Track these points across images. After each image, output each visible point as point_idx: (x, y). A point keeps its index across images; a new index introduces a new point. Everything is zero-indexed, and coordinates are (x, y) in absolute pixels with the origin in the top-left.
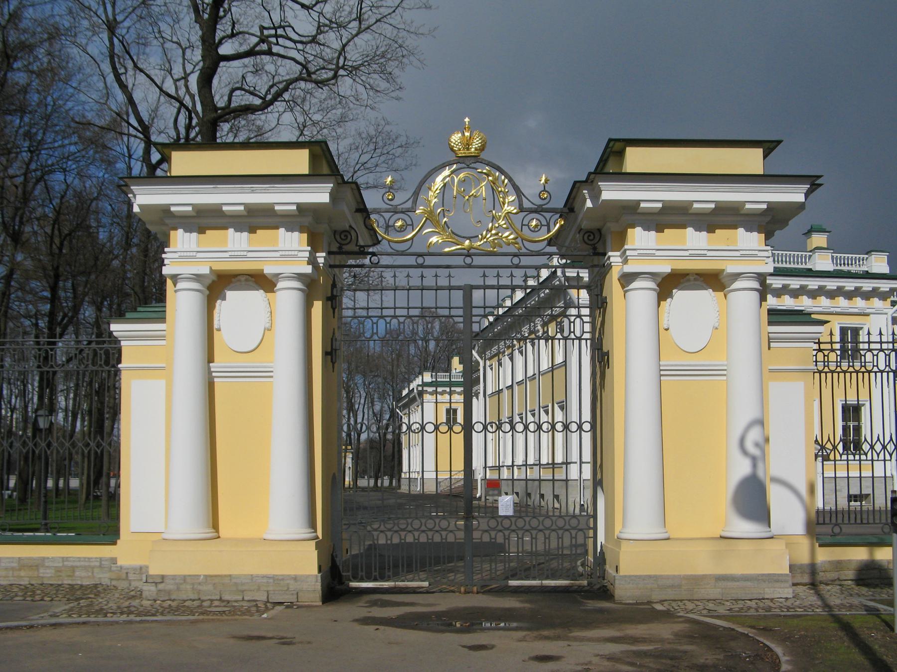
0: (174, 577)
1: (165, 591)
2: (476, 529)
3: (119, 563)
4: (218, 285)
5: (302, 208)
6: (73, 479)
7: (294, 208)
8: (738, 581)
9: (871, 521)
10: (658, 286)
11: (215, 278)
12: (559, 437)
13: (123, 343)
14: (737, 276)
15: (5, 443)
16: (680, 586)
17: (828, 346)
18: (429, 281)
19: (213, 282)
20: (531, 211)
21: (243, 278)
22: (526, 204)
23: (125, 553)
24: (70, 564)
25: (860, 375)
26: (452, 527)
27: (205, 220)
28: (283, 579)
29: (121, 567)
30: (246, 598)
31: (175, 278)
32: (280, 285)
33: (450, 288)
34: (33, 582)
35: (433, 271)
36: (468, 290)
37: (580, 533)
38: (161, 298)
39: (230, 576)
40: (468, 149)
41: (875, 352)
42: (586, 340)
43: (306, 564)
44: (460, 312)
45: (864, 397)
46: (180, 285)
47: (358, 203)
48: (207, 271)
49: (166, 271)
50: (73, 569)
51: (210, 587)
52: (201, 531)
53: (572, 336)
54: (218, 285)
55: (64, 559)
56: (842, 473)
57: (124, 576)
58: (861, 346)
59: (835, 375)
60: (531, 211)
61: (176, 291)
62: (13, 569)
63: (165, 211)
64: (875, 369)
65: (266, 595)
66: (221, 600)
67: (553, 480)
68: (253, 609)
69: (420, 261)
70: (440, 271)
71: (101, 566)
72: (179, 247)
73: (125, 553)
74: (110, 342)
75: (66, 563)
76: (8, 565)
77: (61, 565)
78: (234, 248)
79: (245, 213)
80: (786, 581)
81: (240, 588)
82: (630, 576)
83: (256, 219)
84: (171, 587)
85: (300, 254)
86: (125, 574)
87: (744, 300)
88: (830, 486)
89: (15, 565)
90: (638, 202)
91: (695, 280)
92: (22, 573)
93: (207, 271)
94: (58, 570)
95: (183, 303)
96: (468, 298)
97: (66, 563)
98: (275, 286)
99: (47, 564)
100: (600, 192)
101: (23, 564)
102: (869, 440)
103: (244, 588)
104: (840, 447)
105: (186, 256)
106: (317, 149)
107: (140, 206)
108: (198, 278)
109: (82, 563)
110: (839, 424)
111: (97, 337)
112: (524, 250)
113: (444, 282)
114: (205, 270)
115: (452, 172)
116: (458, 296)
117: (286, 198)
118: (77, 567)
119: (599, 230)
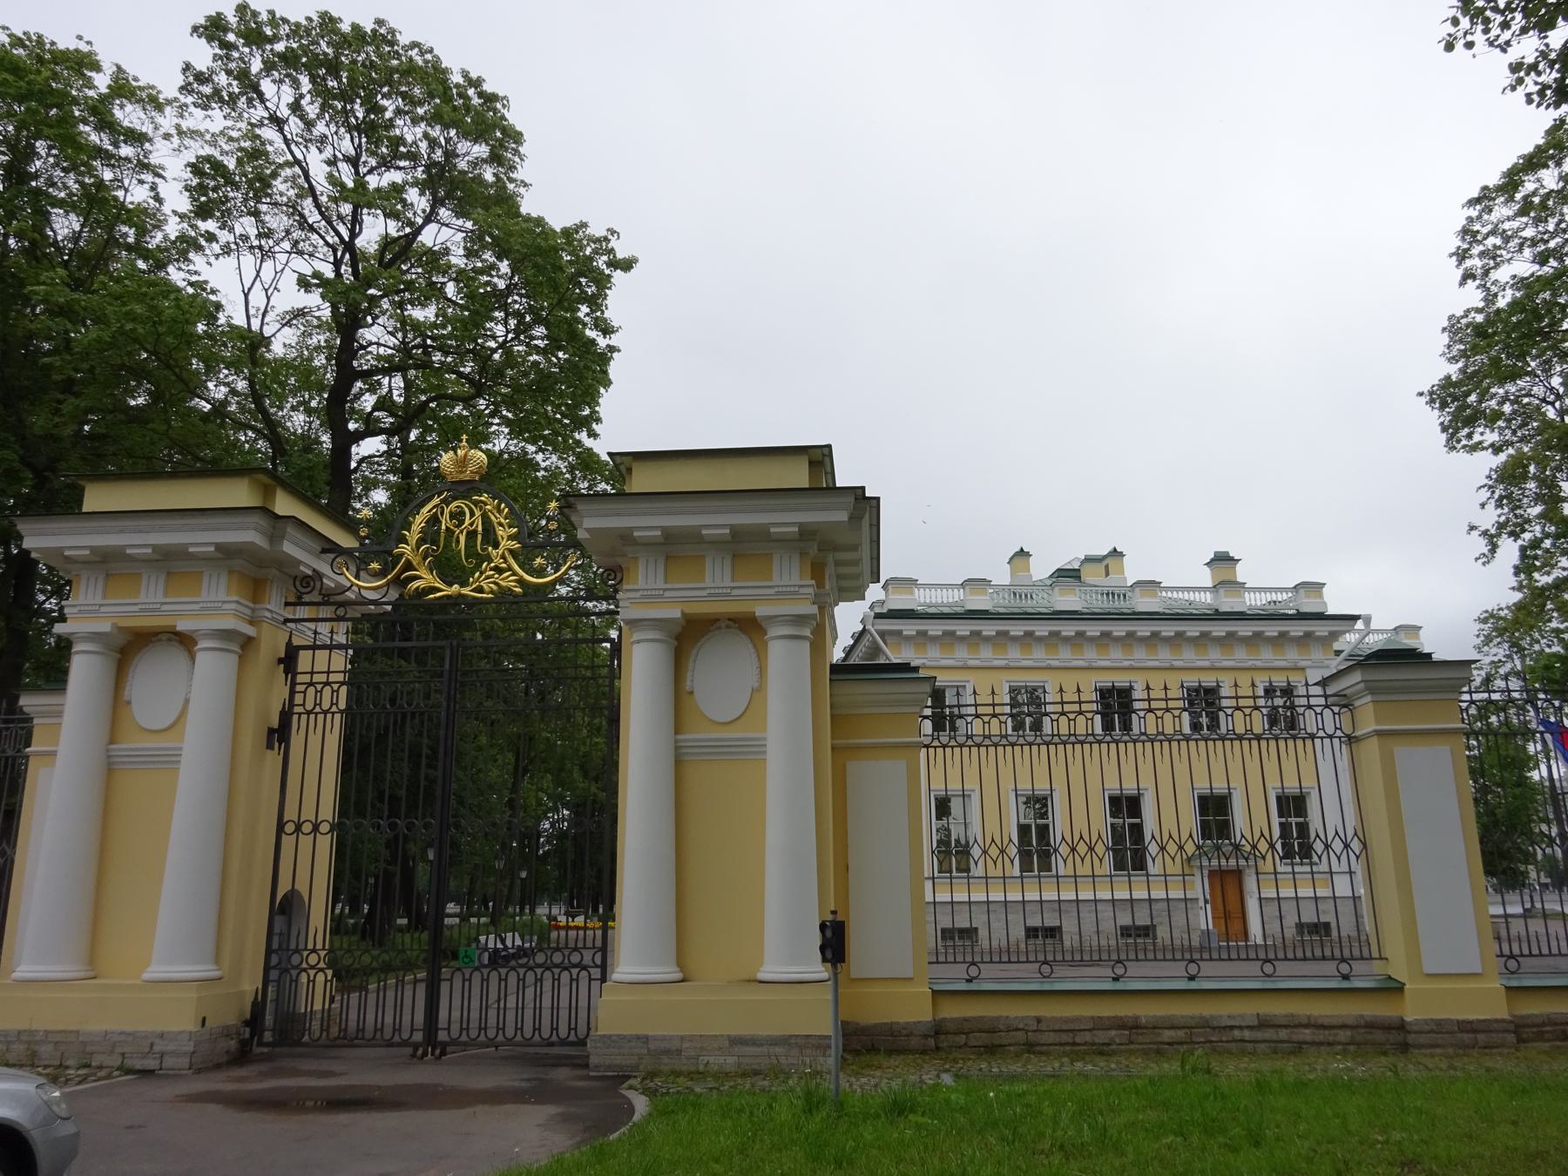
4: (129, 648)
14: (771, 618)
16: (679, 1052)
17: (1250, 702)
21: (164, 637)
37: (584, 973)
41: (1089, 715)
45: (1147, 783)
51: (50, 1048)
52: (670, 972)
53: (318, 709)
56: (1288, 892)
58: (1298, 701)
63: (626, 537)
64: (1321, 733)
67: (1041, 901)
72: (641, 584)
78: (148, 603)
81: (89, 1049)
83: (172, 565)
85: (803, 590)
87: (211, 669)
88: (1271, 910)
90: (631, 529)
91: (728, 627)
95: (84, 670)
100: (283, 537)
102: (1176, 837)
104: (976, 852)
105: (87, 615)
107: (587, 530)
110: (1276, 820)
115: (442, 501)
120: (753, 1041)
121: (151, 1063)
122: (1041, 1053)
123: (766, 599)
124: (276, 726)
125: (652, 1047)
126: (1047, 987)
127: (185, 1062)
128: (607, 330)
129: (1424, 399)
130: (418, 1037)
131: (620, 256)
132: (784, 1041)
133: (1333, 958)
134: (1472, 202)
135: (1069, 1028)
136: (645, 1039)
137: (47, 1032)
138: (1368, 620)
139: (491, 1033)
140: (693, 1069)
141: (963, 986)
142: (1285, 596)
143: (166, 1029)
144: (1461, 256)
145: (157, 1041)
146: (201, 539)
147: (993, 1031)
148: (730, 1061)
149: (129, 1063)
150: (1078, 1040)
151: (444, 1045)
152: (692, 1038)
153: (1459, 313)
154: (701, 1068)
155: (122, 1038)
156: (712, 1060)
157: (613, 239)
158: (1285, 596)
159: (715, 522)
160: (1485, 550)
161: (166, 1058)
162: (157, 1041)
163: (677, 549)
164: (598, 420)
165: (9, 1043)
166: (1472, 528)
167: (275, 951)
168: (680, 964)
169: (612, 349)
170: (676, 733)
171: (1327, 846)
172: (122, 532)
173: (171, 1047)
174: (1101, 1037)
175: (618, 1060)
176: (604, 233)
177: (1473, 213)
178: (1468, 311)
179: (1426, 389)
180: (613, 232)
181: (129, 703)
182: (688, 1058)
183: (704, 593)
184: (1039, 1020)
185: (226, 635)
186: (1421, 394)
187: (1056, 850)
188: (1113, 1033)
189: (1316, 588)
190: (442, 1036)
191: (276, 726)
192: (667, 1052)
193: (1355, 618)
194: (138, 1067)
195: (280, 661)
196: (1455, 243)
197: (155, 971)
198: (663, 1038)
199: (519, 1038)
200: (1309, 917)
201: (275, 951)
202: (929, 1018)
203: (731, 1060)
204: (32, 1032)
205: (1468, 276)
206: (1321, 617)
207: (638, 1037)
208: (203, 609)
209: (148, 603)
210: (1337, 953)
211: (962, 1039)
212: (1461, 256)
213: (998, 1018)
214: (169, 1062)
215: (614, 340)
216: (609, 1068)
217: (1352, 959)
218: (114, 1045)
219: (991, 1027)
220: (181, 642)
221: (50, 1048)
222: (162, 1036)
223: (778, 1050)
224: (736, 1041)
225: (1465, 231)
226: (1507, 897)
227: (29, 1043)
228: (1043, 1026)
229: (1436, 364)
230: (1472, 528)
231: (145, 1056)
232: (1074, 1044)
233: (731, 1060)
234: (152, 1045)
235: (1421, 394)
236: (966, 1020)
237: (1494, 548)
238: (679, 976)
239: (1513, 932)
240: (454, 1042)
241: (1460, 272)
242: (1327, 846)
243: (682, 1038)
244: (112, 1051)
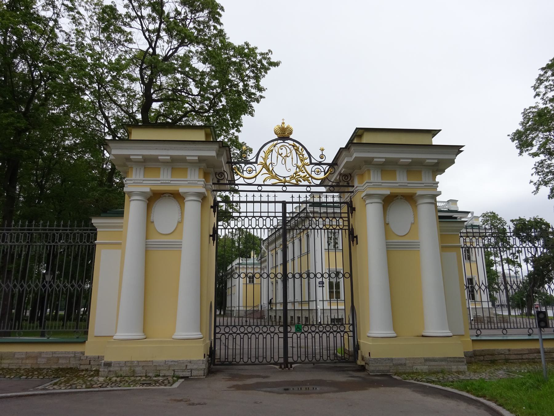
0: (119, 363)
1: (113, 371)
2: (289, 332)
3: (86, 355)
4: (153, 198)
5: (201, 160)
6: (67, 304)
7: (169, 158)
8: (437, 361)
9: (522, 327)
10: (383, 201)
11: (151, 194)
12: (298, 281)
13: (98, 230)
14: (422, 196)
15: (3, 286)
16: (405, 364)
18: (264, 199)
19: (151, 197)
20: (316, 164)
21: (167, 195)
22: (313, 161)
23: (90, 349)
24: (56, 355)
25: (476, 249)
26: (277, 331)
27: (149, 164)
28: (183, 363)
29: (87, 357)
30: (161, 375)
31: (130, 194)
32: (188, 198)
33: (275, 202)
34: (33, 366)
35: (252, 193)
36: (284, 204)
38: (122, 205)
39: (152, 361)
40: (284, 133)
42: (345, 230)
43: (197, 355)
44: (281, 214)
46: (133, 198)
47: (228, 159)
48: (149, 191)
49: (125, 189)
50: (58, 358)
51: (140, 368)
52: (390, 333)
54: (153, 198)
55: (53, 353)
57: (88, 362)
59: (476, 249)
60: (316, 164)
61: (130, 201)
62: (22, 359)
63: (127, 158)
65: (173, 372)
66: (146, 376)
68: (166, 382)
69: (260, 188)
70: (270, 194)
71: (75, 357)
73: (90, 349)
74: (91, 230)
75: (54, 355)
76: (19, 356)
77: (51, 356)
78: (164, 180)
79: (170, 161)
80: (463, 362)
81: (158, 368)
82: (377, 359)
83: (177, 164)
84: (117, 369)
86: (90, 361)
87: (192, 207)
89: (23, 356)
90: (373, 158)
91: (401, 199)
92: (27, 361)
93: (149, 191)
94: (49, 359)
95: (134, 209)
96: (284, 208)
97: (54, 355)
98: (184, 199)
99: (42, 356)
101: (28, 356)
102: (478, 283)
103: (160, 368)
105: (136, 184)
106: (208, 130)
108: (142, 194)
109: (64, 355)
111: (21, 227)
112: (312, 184)
113: (272, 199)
114: (147, 189)
116: (279, 207)
117: (192, 154)
118: (60, 357)
119: (350, 174)
120: (434, 360)
121: (187, 374)
122: (512, 363)
123: (422, 188)
124: (212, 234)
125: (394, 362)
126: (505, 338)
127: (202, 373)
128: (260, 89)
129: (509, 137)
130: (281, 360)
131: (272, 60)
132: (445, 359)
133: (475, 329)
134: (543, 69)
135: (520, 353)
136: (391, 360)
137: (138, 362)
138: (472, 213)
139: (261, 359)
140: (411, 371)
141: (527, 337)
142: (443, 204)
143: (192, 359)
144: (535, 88)
145: (188, 364)
146: (192, 154)
147: (492, 355)
148: (425, 368)
149: (177, 374)
150: (524, 357)
151: (291, 364)
152: (409, 359)
153: (528, 108)
154: (415, 371)
155: (173, 363)
156: (418, 367)
157: (270, 54)
158: (443, 204)
159: (406, 157)
160: (535, 189)
161: (193, 371)
162: (188, 364)
163: (387, 168)
164: (241, 125)
165: (121, 367)
166: (531, 182)
167: (217, 326)
168: (144, 331)
169: (261, 97)
170: (386, 240)
171: (480, 288)
172: (156, 149)
173: (195, 367)
174: (532, 356)
175: (381, 368)
176: (268, 51)
177: (542, 73)
178: (530, 108)
179: (511, 133)
180: (270, 51)
181: (153, 222)
182: (409, 367)
183: (397, 185)
184: (509, 350)
185: (198, 194)
186: (509, 135)
187: (486, 287)
188: (536, 355)
189: (455, 202)
190: (290, 360)
191: (212, 234)
192: (401, 365)
193: (468, 213)
194: (181, 376)
195: (212, 207)
196: (534, 82)
197: (180, 334)
198: (399, 359)
199: (307, 360)
200: (334, 315)
201: (217, 326)
202: (472, 350)
203: (426, 367)
204: (132, 362)
205: (538, 95)
206: (457, 212)
207: (389, 359)
208: (189, 183)
209: (164, 180)
210: (529, 327)
211: (482, 358)
212: (535, 88)
213: (494, 350)
214: (195, 373)
215: (263, 94)
216: (378, 371)
217: (508, 328)
218: (170, 366)
219: (492, 353)
220: (174, 197)
221: (140, 368)
222: (190, 362)
223: (443, 363)
224: (427, 360)
225: (538, 79)
226: (503, 309)
227: (130, 366)
228: (511, 353)
229: (515, 124)
230: (531, 182)
231: (183, 371)
232: (522, 359)
233: (426, 367)
234: (186, 366)
235: (509, 135)
236: (483, 351)
237: (538, 189)
238: (144, 337)
239: (512, 321)
240: (295, 362)
241: (535, 93)
242: (480, 288)
243: (406, 359)
244: (169, 369)
